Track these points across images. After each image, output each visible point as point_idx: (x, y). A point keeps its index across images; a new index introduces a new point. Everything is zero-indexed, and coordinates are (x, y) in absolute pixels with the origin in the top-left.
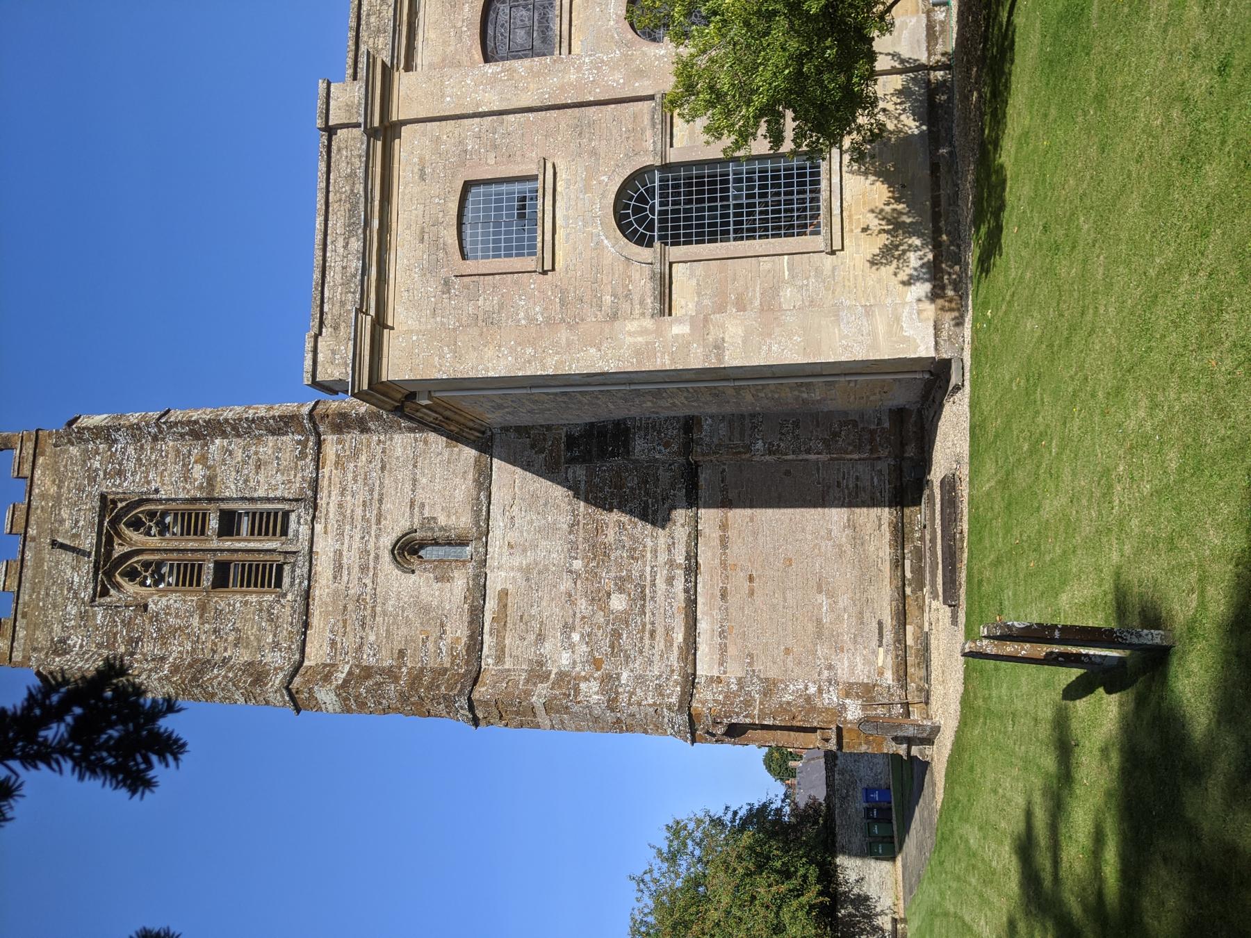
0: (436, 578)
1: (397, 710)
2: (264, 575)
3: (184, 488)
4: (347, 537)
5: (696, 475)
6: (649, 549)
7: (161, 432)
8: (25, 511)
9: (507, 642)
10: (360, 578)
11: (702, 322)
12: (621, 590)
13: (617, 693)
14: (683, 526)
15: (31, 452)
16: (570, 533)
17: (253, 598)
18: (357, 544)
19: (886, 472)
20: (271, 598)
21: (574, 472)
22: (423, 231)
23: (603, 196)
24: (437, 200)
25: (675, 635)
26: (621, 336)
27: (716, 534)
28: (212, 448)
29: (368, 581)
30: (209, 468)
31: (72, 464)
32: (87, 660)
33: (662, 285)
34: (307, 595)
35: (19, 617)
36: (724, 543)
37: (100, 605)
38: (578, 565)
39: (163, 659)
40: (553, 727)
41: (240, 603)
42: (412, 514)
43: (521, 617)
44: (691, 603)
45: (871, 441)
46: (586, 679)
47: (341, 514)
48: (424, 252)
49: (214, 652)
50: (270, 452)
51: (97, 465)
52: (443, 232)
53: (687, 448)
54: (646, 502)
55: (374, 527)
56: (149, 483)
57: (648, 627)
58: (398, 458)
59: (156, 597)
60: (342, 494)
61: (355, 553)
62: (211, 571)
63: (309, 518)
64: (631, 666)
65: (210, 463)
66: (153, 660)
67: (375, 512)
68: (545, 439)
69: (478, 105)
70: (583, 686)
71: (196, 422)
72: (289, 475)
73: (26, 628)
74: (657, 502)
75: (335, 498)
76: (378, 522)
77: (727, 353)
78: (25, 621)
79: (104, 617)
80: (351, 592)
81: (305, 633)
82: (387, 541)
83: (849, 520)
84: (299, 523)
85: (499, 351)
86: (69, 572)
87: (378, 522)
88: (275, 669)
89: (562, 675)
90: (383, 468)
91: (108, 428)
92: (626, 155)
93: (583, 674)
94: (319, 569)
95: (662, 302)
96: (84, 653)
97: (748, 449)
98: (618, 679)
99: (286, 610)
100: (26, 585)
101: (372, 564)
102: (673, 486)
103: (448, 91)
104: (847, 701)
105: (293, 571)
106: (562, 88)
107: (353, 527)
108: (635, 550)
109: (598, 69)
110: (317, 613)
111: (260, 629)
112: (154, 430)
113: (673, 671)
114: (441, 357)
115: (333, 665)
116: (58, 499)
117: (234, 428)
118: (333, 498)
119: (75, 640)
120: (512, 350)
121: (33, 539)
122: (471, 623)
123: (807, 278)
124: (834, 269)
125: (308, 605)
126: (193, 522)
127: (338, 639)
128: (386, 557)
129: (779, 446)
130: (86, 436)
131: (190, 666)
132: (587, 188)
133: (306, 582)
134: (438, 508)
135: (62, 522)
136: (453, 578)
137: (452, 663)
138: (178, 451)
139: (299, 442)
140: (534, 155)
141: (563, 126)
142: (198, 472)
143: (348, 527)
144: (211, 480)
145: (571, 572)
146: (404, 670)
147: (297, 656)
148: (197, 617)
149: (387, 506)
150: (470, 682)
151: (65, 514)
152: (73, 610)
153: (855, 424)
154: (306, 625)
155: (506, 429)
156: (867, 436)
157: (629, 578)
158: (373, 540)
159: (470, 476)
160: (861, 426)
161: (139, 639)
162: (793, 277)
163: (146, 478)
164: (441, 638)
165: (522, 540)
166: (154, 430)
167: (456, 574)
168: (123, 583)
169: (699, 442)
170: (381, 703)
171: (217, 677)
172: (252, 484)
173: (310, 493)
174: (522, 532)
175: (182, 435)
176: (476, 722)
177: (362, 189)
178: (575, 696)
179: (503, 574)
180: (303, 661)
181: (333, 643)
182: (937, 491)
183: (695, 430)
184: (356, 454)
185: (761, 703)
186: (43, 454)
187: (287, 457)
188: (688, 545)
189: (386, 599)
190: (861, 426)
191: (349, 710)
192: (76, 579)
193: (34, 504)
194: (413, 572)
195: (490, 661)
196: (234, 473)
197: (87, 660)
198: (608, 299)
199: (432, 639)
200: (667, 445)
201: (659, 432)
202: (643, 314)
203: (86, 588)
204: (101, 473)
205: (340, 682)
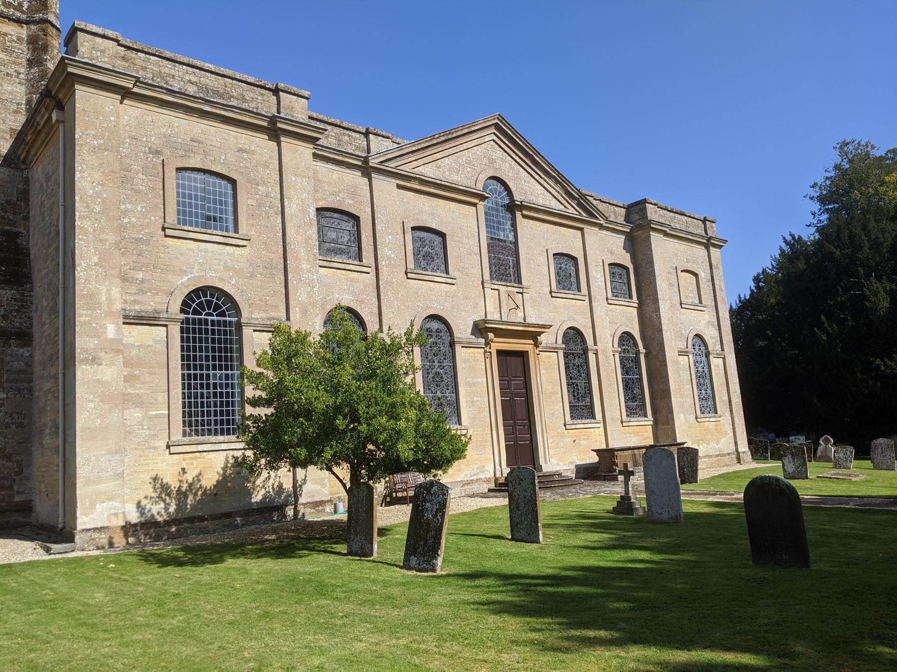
11: (116, 347)
22: (199, 142)
23: (221, 279)
48: (183, 140)
77: (89, 367)
85: (98, 184)
92: (250, 298)
106: (297, 258)
109: (309, 284)
120: (98, 195)
123: (148, 428)
141: (273, 256)
155: (26, 181)
162: (151, 418)
190: (17, 478)
198: (140, 275)
202: (125, 302)
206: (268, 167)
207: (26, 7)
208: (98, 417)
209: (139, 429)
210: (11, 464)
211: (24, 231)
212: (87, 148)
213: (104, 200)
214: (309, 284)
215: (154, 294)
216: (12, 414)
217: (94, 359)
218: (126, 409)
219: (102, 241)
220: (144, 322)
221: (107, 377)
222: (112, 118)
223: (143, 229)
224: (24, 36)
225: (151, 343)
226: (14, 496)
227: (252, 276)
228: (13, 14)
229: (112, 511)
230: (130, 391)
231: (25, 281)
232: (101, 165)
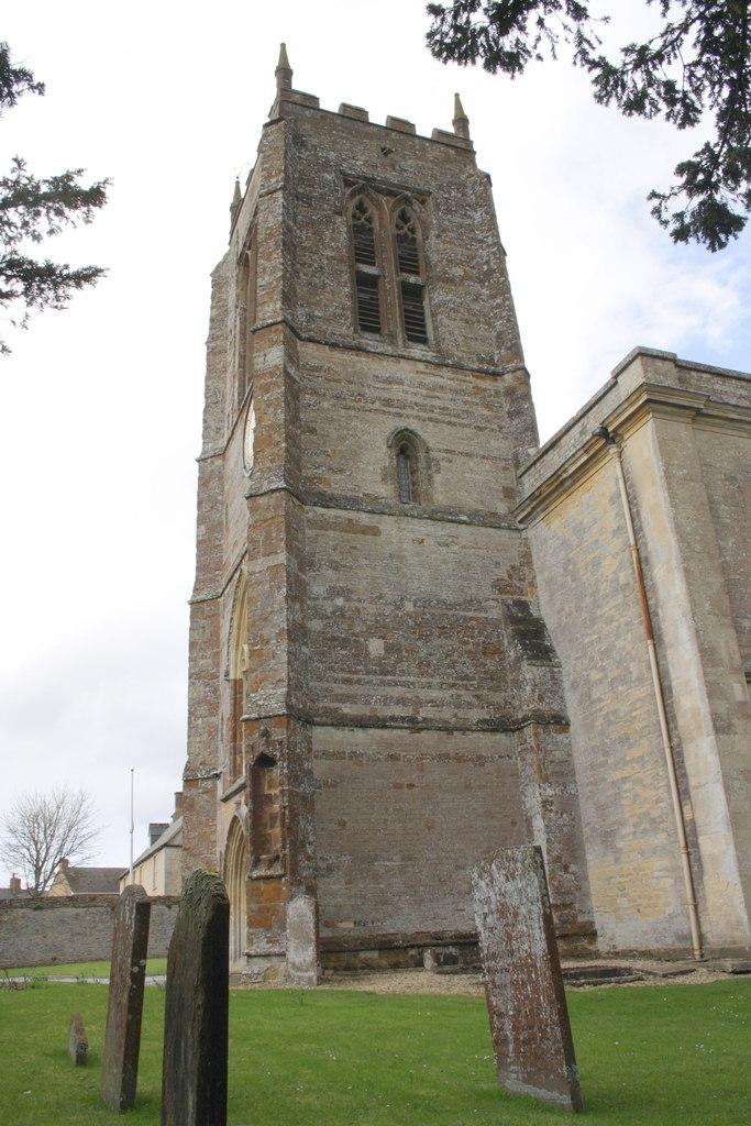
2: (368, 318)
18: (411, 398)
21: (494, 607)
36: (444, 757)
54: (473, 679)
61: (401, 396)
81: (326, 344)
82: (414, 425)
90: (479, 428)
121: (387, 135)
126: (410, 260)
128: (402, 424)
142: (458, 272)
144: (451, 281)
145: (402, 599)
158: (415, 413)
172: (453, 315)
181: (318, 369)
195: (311, 515)
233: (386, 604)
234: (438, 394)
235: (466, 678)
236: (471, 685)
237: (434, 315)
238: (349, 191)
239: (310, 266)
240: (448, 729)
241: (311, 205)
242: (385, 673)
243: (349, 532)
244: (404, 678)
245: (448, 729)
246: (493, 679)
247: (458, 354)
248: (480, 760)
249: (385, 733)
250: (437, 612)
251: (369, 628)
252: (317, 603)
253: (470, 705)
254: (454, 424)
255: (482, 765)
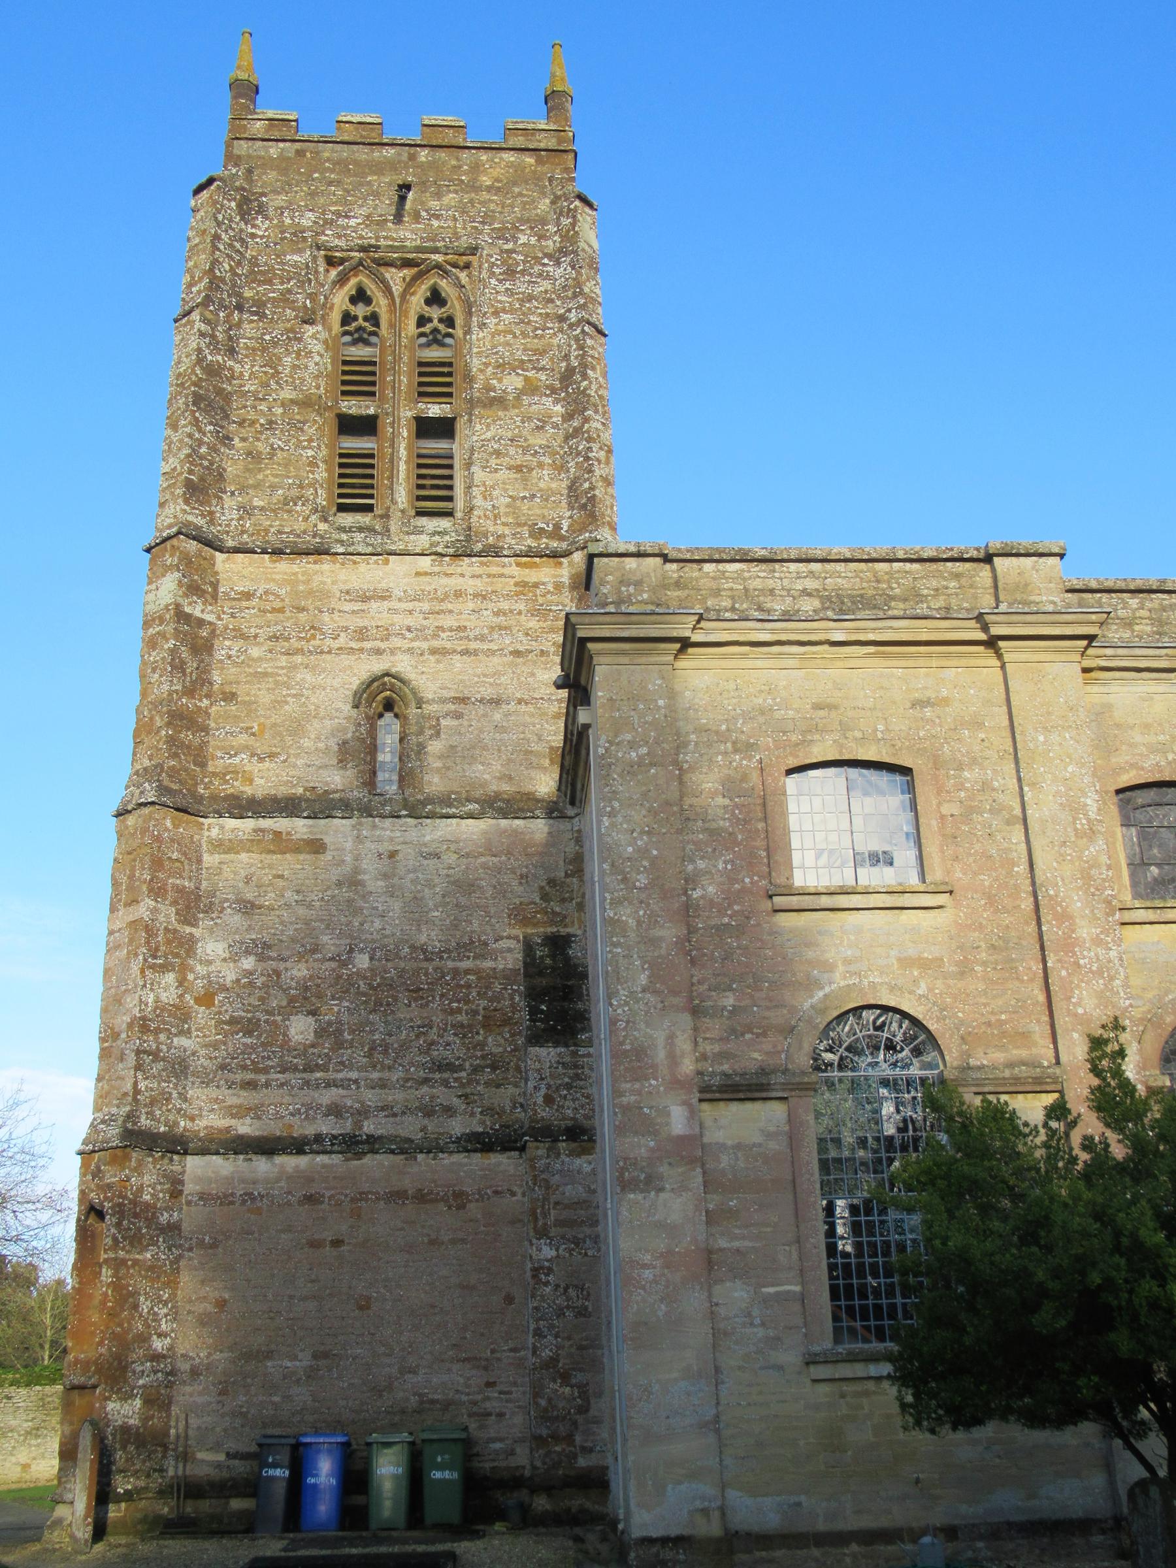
0: (345, 743)
1: (144, 694)
2: (355, 487)
3: (486, 365)
4: (410, 606)
5: (505, 1149)
6: (386, 1075)
7: (571, 326)
8: (454, 143)
9: (244, 856)
10: (347, 629)
11: (692, 1150)
12: (321, 1033)
13: (157, 1031)
14: (423, 1129)
15: (542, 145)
16: (413, 948)
17: (321, 474)
18: (401, 620)
19: (513, 1462)
20: (322, 501)
21: (510, 950)
22: (832, 707)
23: (892, 989)
24: (881, 727)
25: (248, 1120)
26: (667, 1023)
27: (408, 1184)
28: (548, 402)
29: (342, 640)
30: (518, 398)
31: (525, 203)
32: (231, 246)
33: (750, 1088)
34: (321, 551)
35: (297, 146)
36: (397, 1196)
37: (315, 258)
38: (362, 961)
39: (232, 352)
40: (111, 933)
41: (312, 455)
42: (443, 701)
43: (281, 877)
44: (298, 1146)
45: (555, 1437)
46: (181, 982)
47: (446, 595)
48: (798, 711)
49: (241, 424)
50: (542, 485)
51: (523, 239)
52: (829, 739)
53: (545, 1133)
54: (461, 1068)
55: (425, 645)
56: (496, 313)
57: (263, 1079)
58: (533, 675)
59: (324, 335)
60: (476, 596)
61: (385, 619)
62: (363, 412)
63: (439, 549)
64: (202, 1052)
65: (526, 400)
66: (230, 338)
67: (448, 645)
68: (563, 900)
69: (1033, 785)
70: (170, 978)
71: (585, 376)
72: (507, 514)
73: (282, 158)
74: (462, 1086)
75: (471, 585)
76: (434, 651)
77: (640, 1197)
78: (291, 155)
79: (295, 266)
80: (326, 617)
81: (264, 552)
82: (403, 665)
83: (433, 1402)
84: (434, 533)
85: (642, 832)
86: (364, 211)
87: (434, 651)
88: (211, 513)
89: (190, 945)
90: (517, 653)
91: (575, 252)
92: (962, 1022)
93: (191, 977)
94: (363, 567)
95: (723, 1089)
96: (242, 241)
97: (542, 1233)
98: (181, 1033)
99: (301, 523)
100: (345, 152)
101: (368, 645)
102: (488, 1111)
103: (1055, 738)
104: (138, 1403)
105: (361, 529)
106: (1065, 917)
107: (426, 615)
108: (385, 1052)
109: (1100, 973)
110: (295, 568)
111: (273, 487)
112: (573, 316)
113: (192, 1119)
114: (632, 745)
115: (215, 597)
116: (474, 187)
117: (577, 431)
118: (471, 582)
119: (262, 227)
120: (643, 852)
121: (412, 157)
122: (275, 800)
123: (763, 1324)
124: (780, 1368)
125: (308, 554)
126: (436, 379)
127: (255, 602)
128: (378, 666)
129: (547, 1284)
130: (565, 221)
131: (219, 392)
132: (906, 962)
133: (341, 550)
134: (455, 741)
135: (438, 195)
136: (344, 768)
137: (214, 774)
138: (543, 353)
139: (557, 527)
140: (958, 875)
141: (1007, 919)
142: (512, 383)
143: (426, 606)
144: (500, 402)
145: (351, 951)
146: (206, 702)
147: (230, 543)
148: (293, 395)
149: (458, 662)
150: (180, 801)
151: (450, 198)
152: (307, 219)
153: (584, 1409)
154: (277, 552)
155: (579, 840)
156: (563, 1429)
157: (339, 1045)
158: (406, 644)
159: (505, 787)
160: (580, 1419)
161: (262, 316)
162: (766, 1301)
163: (504, 311)
164: (253, 755)
165: (401, 871)
166: (573, 316)
167: (350, 773)
168: (346, 288)
169: (553, 1152)
170: (154, 670)
171: (200, 430)
172: (493, 462)
173: (479, 547)
174: (415, 871)
175: (566, 357)
176: (121, 814)
177: (896, 613)
178: (152, 967)
179: (349, 845)
180: (221, 552)
181: (248, 596)
182: (447, 1546)
183: (574, 1145)
184: (539, 612)
185: (136, 1262)
186: (539, 161)
187: (533, 510)
188: (392, 1139)
189: (314, 668)
190: (580, 1419)
191: (147, 624)
192: (353, 222)
193: (465, 155)
194: (356, 706)
195: (215, 832)
196: (510, 434)
197: (231, 246)
198: (729, 1001)
199: (251, 741)
200: (549, 1100)
201: (568, 1087)
202: (704, 1057)
203: (339, 237)
204: (510, 246)
205: (188, 610)
206: (980, 725)
207: (565, 528)
208: (662, 1300)
209: (744, 1325)
210: (567, 1390)
211: (579, 932)
212: (619, 770)
213: (653, 861)
214: (1100, 973)
215: (758, 1035)
216: (566, 1289)
217: (649, 1180)
218: (716, 1282)
219: (654, 942)
220: (741, 1096)
221: (675, 1217)
222: (661, 703)
223: (730, 906)
224: (566, 580)
225: (757, 1138)
226: (575, 1456)
227: (964, 970)
228: (547, 548)
229: (698, 1504)
230: (723, 1243)
231: (579, 1026)
232: (645, 795)
233: (324, 960)
234: (450, 606)
235: (451, 1067)
236: (456, 1080)
237: (468, 465)
238: (333, 273)
239: (253, 423)
240: (406, 1148)
241: (264, 316)
242: (308, 1069)
243: (274, 852)
244: (340, 1076)
245: (406, 1148)
246: (494, 1068)
247: (493, 529)
248: (459, 1199)
249: (302, 1161)
250: (409, 966)
251: (292, 1000)
252: (212, 968)
253: (449, 1111)
254: (475, 653)
255: (461, 1207)
